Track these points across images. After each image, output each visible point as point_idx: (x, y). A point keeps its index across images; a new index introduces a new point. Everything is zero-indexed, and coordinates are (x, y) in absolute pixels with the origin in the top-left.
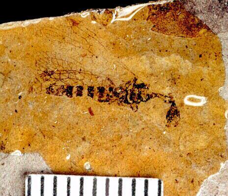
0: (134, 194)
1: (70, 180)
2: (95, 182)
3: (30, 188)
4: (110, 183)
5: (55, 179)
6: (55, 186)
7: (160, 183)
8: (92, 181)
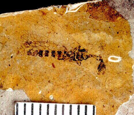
0: (78, 114)
1: (41, 106)
2: (56, 107)
3: (18, 110)
4: (65, 108)
5: (32, 105)
6: (32, 109)
7: (94, 107)
8: (54, 106)
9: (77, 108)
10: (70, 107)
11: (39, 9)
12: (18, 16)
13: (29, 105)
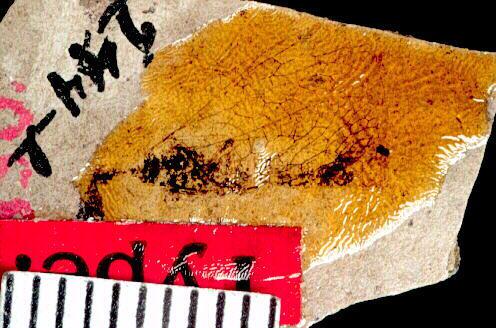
0: (219, 322)
2: (143, 295)
3: (11, 298)
4: (228, 300)
6: (89, 301)
9: (216, 302)
10: (192, 298)
11: (374, 30)
12: (426, 61)
13: (234, 299)
